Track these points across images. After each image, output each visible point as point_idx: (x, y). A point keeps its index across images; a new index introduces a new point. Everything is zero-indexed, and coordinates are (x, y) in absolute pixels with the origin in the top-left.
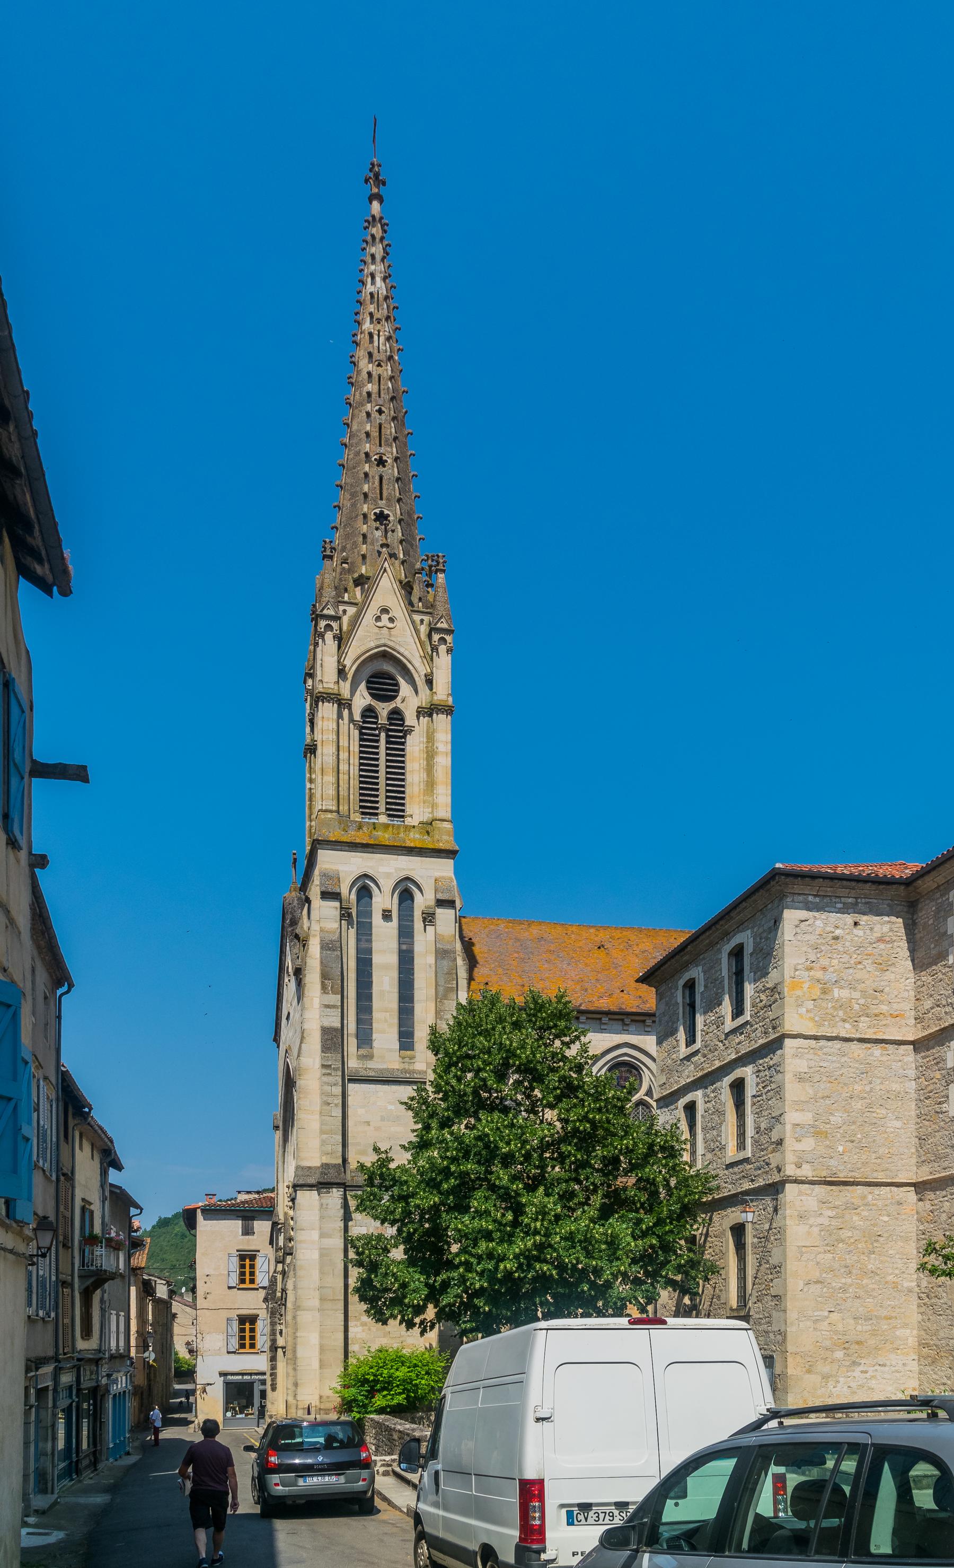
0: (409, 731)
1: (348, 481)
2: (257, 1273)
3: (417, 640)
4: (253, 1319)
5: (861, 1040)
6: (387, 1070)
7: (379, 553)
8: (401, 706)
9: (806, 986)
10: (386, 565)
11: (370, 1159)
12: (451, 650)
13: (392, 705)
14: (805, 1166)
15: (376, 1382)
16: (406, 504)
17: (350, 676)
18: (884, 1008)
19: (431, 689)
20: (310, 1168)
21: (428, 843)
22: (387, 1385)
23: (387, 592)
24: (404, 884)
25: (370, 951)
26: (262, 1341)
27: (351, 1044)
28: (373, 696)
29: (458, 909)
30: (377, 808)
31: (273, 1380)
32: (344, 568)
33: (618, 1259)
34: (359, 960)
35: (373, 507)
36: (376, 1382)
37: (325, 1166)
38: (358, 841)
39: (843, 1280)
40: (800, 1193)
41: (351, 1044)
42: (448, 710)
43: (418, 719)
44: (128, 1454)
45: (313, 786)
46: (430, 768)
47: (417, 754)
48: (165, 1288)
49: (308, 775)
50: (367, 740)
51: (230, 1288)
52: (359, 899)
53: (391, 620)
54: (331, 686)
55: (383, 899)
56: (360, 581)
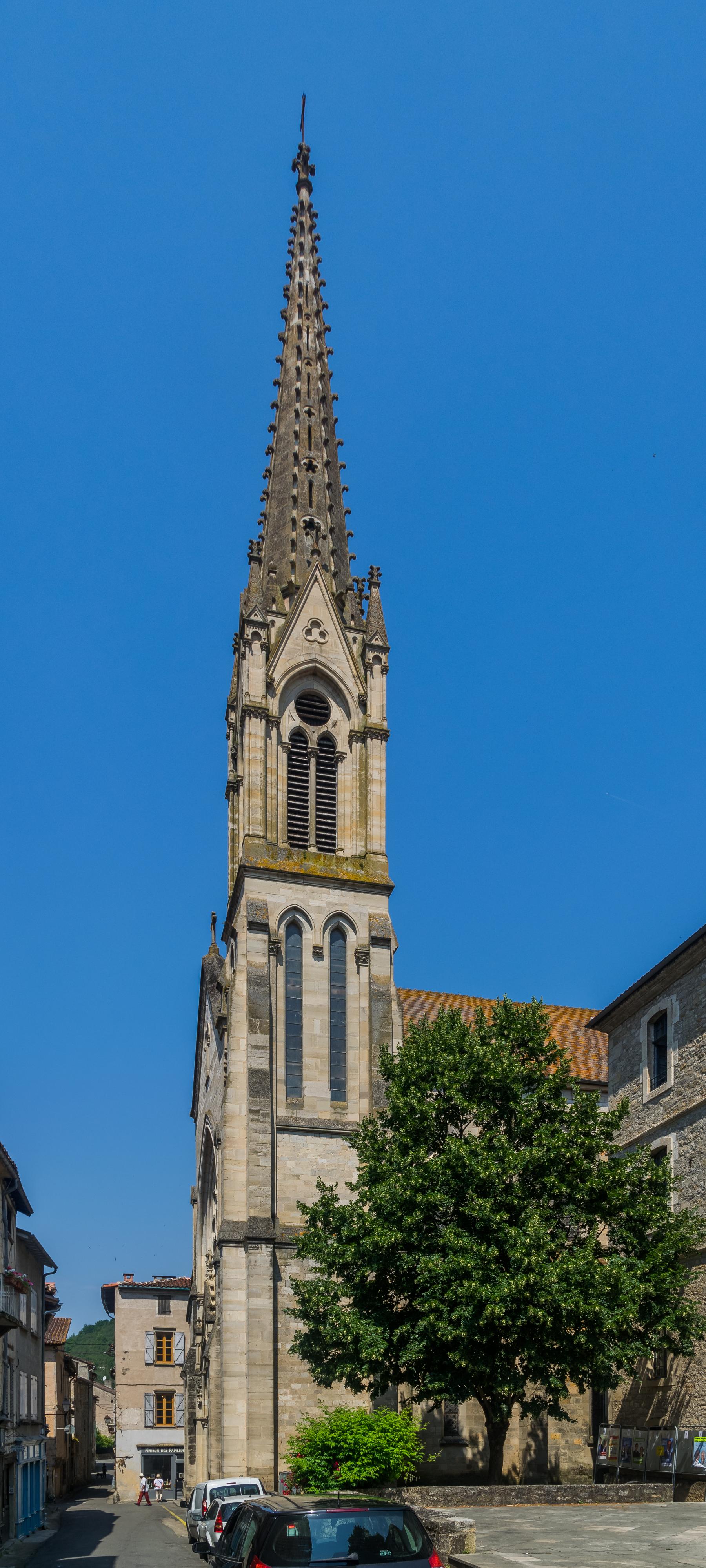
0: (342, 757)
1: (275, 488)
2: (174, 1350)
3: (350, 658)
4: (170, 1395)
6: (318, 1120)
7: (309, 563)
11: (313, 1198)
12: (387, 670)
13: (323, 729)
15: (339, 1449)
17: (279, 691)
19: (365, 711)
20: (236, 1223)
21: (361, 876)
22: (353, 1454)
23: (317, 603)
24: (335, 921)
25: (300, 993)
26: (179, 1415)
27: (280, 1092)
28: (303, 719)
29: (393, 949)
30: (306, 840)
31: (191, 1453)
32: (271, 578)
33: (620, 1306)
34: (287, 1001)
35: (302, 513)
36: (339, 1449)
37: (253, 1220)
38: (288, 869)
41: (280, 1092)
42: (383, 735)
43: (350, 744)
44: (43, 1528)
45: (236, 827)
47: (348, 784)
48: (86, 1370)
50: (297, 769)
51: (147, 1364)
52: (288, 935)
53: (323, 634)
54: (259, 700)
55: (314, 936)
56: (290, 591)
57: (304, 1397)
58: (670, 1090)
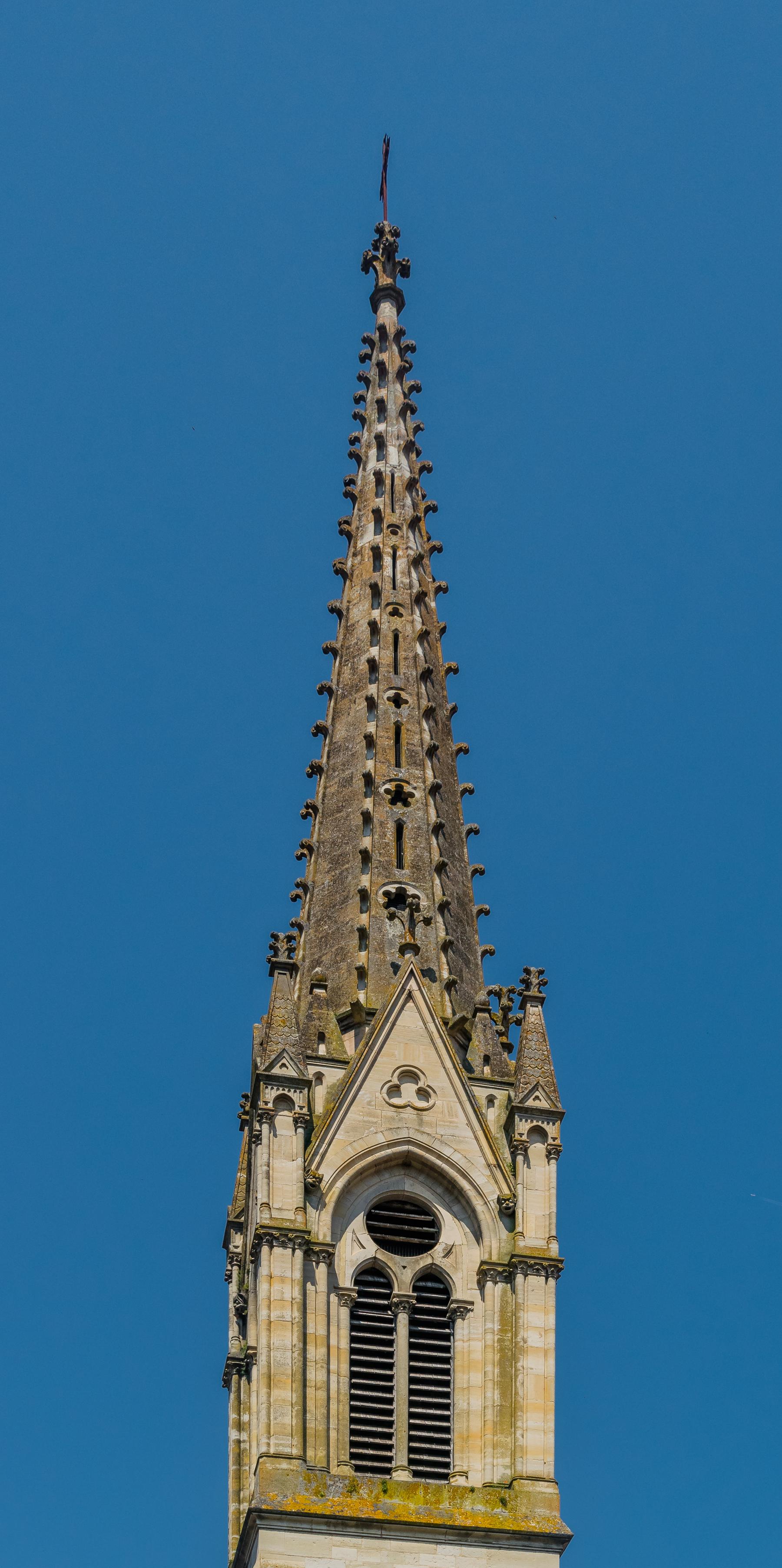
0: (465, 1309)
1: (327, 836)
8: (445, 1264)
10: (412, 984)
12: (558, 1153)
13: (424, 1261)
16: (455, 882)
19: (511, 1228)
21: (503, 1519)
23: (413, 1037)
32: (317, 998)
35: (381, 880)
38: (348, 1513)
42: (550, 1268)
43: (481, 1286)
45: (244, 1436)
47: (477, 1356)
49: (233, 1416)
53: (423, 1093)
54: (290, 1215)
56: (354, 1020)
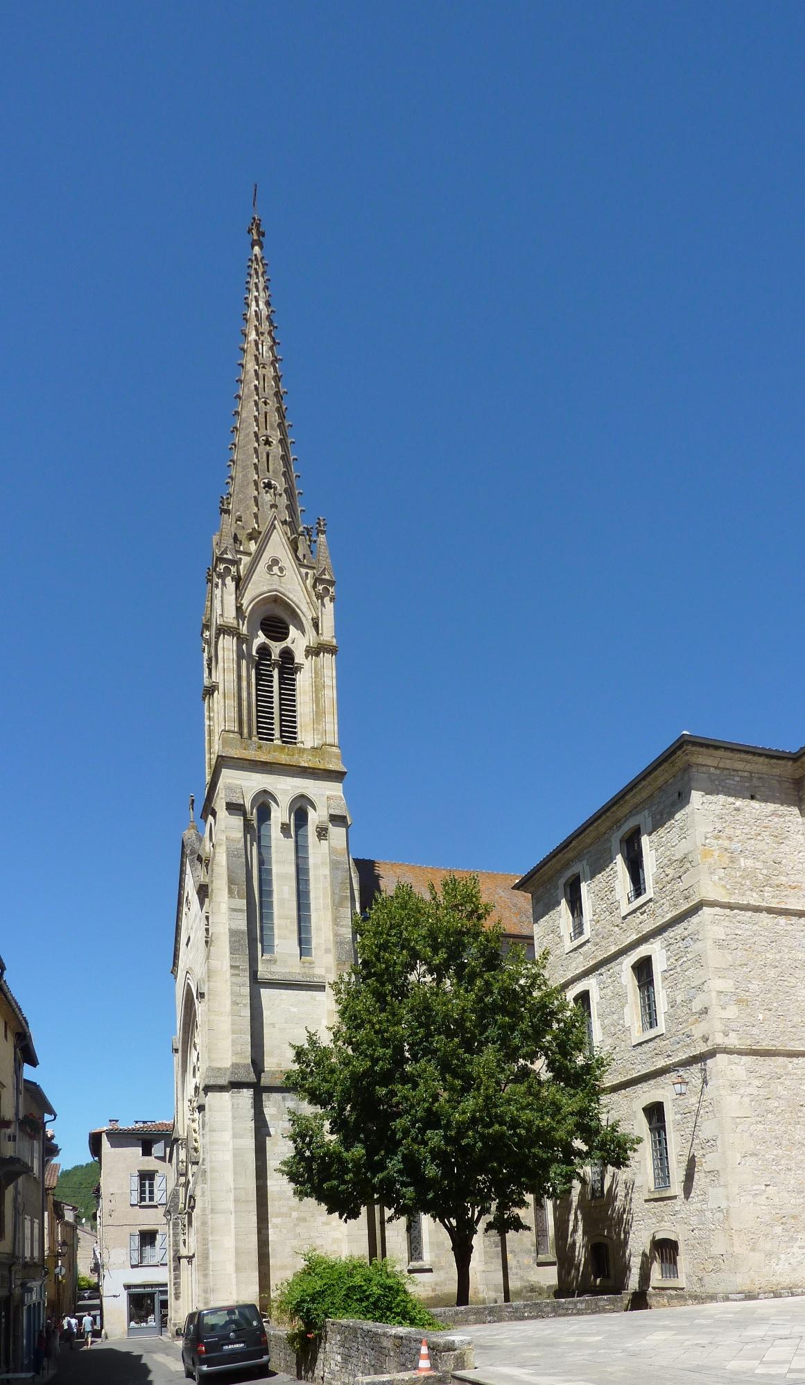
5: (770, 911)
8: (292, 647)
9: (716, 854)
13: (283, 644)
14: (732, 1034)
18: (783, 879)
20: (220, 1069)
23: (278, 546)
28: (267, 636)
39: (775, 1152)
40: (730, 1063)
42: (332, 650)
46: (317, 700)
49: (207, 714)
53: (281, 569)
55: (280, 815)
57: (285, 1231)
58: (588, 941)
